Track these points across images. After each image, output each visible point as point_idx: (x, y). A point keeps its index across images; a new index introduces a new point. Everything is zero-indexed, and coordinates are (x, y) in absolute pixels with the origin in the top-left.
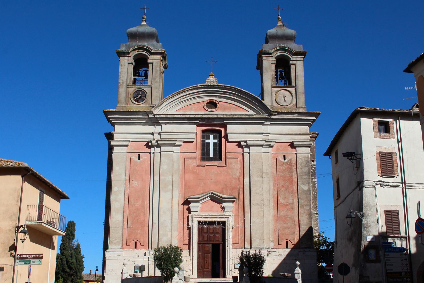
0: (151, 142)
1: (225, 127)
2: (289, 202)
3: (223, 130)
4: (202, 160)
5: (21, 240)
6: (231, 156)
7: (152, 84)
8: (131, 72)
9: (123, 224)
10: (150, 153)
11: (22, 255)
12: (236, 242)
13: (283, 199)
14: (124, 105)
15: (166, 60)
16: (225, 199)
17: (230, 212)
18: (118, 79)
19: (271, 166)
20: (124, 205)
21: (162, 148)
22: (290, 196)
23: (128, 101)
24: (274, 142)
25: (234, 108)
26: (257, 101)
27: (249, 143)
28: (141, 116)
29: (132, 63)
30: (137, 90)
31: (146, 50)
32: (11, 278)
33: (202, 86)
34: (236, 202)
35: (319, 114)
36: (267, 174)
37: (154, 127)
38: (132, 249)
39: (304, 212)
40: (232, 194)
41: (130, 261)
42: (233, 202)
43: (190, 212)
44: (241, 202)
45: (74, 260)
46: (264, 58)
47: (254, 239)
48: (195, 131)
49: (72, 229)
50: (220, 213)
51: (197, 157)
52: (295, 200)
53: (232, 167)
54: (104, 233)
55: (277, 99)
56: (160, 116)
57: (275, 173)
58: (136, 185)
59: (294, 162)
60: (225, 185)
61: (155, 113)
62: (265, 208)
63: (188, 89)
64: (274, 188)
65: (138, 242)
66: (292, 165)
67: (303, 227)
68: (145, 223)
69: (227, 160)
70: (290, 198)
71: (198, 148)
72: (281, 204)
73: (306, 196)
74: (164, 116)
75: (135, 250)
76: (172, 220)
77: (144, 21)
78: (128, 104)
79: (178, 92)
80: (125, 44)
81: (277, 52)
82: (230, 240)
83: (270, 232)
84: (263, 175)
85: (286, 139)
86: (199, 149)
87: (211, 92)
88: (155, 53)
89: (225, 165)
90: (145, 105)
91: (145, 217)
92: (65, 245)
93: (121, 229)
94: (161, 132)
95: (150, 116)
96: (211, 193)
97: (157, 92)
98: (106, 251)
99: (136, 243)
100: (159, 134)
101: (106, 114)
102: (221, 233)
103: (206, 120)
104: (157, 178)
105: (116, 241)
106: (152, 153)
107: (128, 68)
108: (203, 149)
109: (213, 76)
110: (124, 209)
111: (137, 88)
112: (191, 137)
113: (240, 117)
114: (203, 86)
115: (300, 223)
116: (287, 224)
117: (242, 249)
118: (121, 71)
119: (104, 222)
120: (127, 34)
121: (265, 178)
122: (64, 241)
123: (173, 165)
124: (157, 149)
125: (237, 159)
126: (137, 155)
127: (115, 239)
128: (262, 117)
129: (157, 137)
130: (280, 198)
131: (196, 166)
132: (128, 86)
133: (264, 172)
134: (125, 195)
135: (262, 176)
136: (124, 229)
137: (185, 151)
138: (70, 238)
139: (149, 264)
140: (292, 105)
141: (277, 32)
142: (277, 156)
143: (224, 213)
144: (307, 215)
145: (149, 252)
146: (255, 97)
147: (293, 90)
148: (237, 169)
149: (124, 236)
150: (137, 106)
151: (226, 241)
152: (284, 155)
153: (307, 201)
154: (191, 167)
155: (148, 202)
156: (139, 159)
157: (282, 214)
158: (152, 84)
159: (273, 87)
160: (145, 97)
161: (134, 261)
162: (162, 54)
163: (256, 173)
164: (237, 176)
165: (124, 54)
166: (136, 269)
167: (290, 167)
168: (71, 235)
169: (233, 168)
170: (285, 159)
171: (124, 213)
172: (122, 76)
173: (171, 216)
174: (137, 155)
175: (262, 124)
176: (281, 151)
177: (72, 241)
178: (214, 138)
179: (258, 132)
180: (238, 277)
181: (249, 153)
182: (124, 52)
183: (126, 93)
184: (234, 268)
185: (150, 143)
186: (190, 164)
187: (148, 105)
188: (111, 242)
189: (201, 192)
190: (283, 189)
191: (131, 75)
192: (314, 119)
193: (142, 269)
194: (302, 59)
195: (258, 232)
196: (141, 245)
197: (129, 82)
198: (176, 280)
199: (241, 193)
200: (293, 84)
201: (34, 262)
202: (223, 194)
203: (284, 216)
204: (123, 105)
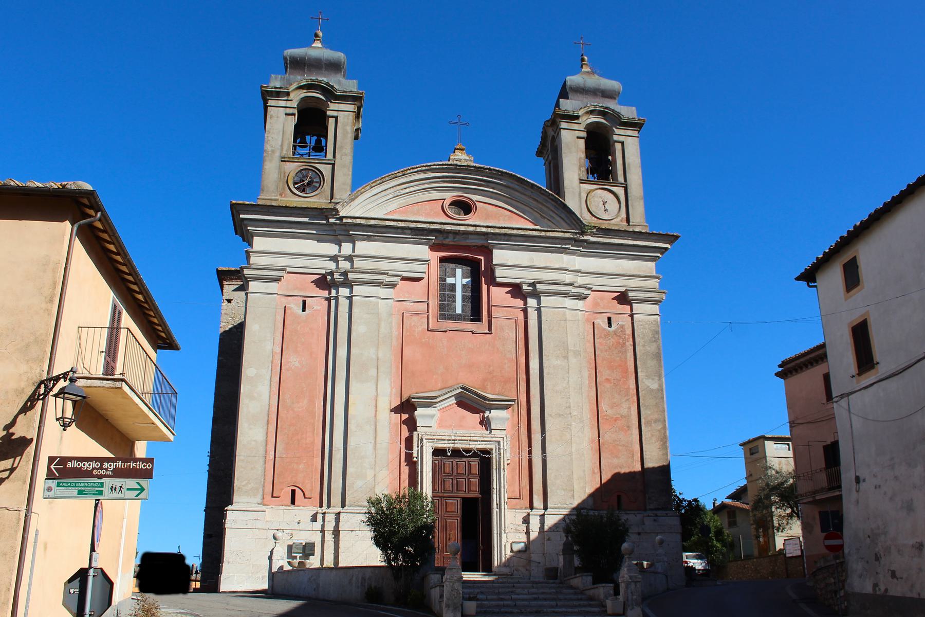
2: (621, 413)
4: (439, 319)
5: (57, 420)
9: (266, 449)
10: (329, 299)
11: (71, 459)
13: (608, 405)
14: (274, 196)
16: (491, 403)
18: (264, 143)
19: (582, 337)
20: (269, 409)
23: (284, 189)
24: (590, 289)
25: (506, 216)
26: (555, 204)
27: (539, 287)
30: (302, 168)
32: (14, 557)
34: (513, 410)
36: (577, 354)
38: (285, 506)
39: (652, 436)
40: (504, 392)
44: (523, 410)
46: (563, 125)
47: (553, 488)
48: (427, 258)
50: (479, 432)
51: (430, 311)
53: (503, 336)
54: (209, 475)
55: (590, 205)
56: (354, 221)
58: (297, 364)
59: (629, 331)
60: (490, 373)
61: (342, 214)
62: (573, 423)
63: (414, 171)
65: (298, 491)
66: (625, 337)
68: (315, 449)
72: (605, 417)
74: (363, 222)
75: (292, 507)
76: (376, 444)
77: (318, 40)
78: (283, 196)
79: (392, 174)
80: (280, 76)
81: (588, 115)
82: (502, 489)
83: (585, 475)
84: (569, 354)
85: (613, 284)
86: (433, 295)
88: (344, 98)
89: (487, 331)
90: (319, 199)
91: (315, 435)
93: (262, 461)
95: (332, 220)
96: (462, 388)
98: (226, 508)
99: (293, 492)
100: (350, 259)
101: (236, 209)
108: (442, 298)
109: (462, 150)
111: (303, 164)
114: (445, 167)
117: (528, 511)
118: (270, 129)
119: (208, 452)
120: (285, 59)
121: (573, 360)
123: (379, 325)
124: (344, 291)
125: (514, 321)
127: (246, 481)
129: (344, 265)
130: (604, 405)
131: (428, 331)
132: (283, 160)
134: (272, 386)
135: (566, 357)
137: (405, 297)
140: (619, 219)
141: (585, 81)
142: (595, 319)
146: (552, 195)
147: (620, 191)
148: (515, 339)
150: (302, 199)
153: (657, 412)
154: (416, 332)
156: (304, 310)
160: (318, 184)
162: (356, 99)
165: (278, 94)
167: (621, 341)
170: (610, 325)
171: (268, 424)
172: (272, 138)
176: (603, 308)
179: (557, 266)
182: (279, 90)
183: (280, 173)
186: (414, 325)
187: (326, 199)
188: (239, 488)
189: (439, 386)
190: (608, 385)
191: (290, 137)
192: (666, 249)
193: (308, 550)
194: (636, 134)
197: (286, 151)
200: (621, 179)
201: (118, 490)
202: (485, 391)
203: (612, 442)
204: (272, 196)
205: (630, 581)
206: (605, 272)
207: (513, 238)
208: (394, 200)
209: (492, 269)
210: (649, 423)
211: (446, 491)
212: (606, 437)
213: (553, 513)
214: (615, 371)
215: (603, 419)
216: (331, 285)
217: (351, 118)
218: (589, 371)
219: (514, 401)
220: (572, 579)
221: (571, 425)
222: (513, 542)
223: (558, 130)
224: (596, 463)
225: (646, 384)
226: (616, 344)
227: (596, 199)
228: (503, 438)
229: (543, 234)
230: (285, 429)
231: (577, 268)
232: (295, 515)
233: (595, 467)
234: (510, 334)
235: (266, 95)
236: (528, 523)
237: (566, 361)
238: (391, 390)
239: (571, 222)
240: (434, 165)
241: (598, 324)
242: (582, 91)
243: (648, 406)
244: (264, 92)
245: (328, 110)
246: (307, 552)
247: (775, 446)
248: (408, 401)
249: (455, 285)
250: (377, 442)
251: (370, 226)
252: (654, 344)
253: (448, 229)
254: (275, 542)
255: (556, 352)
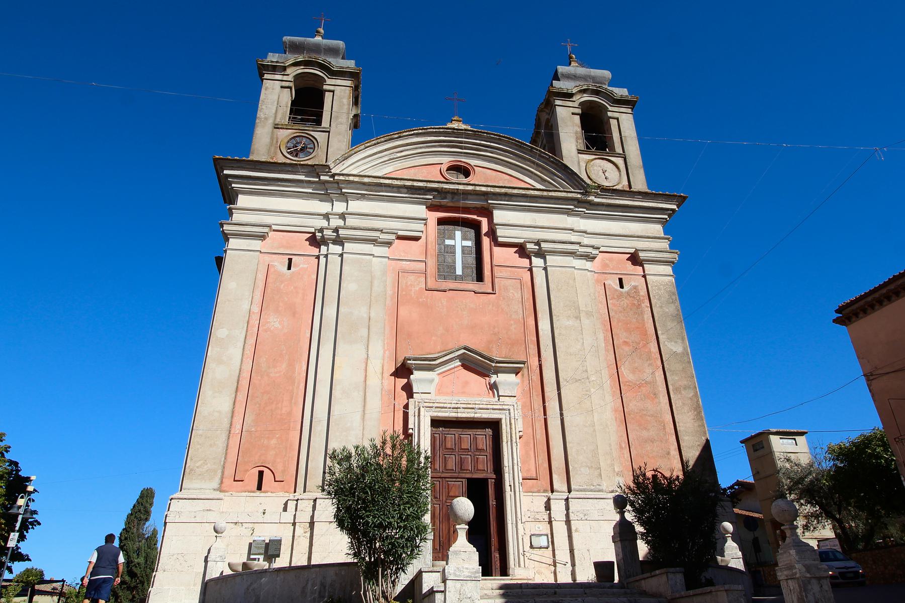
0: (321, 230)
1: (489, 215)
3: (484, 222)
6: (504, 273)
7: (330, 126)
8: (287, 103)
10: (318, 257)
12: (528, 476)
13: (629, 370)
15: (360, 105)
17: (511, 396)
19: (594, 298)
20: (240, 374)
21: (348, 246)
22: (646, 365)
23: (275, 153)
26: (556, 167)
28: (302, 177)
29: (290, 88)
31: (322, 67)
33: (440, 130)
34: (523, 375)
35: (684, 198)
36: (589, 314)
37: (329, 203)
38: (249, 492)
39: (684, 404)
41: (238, 527)
42: (517, 372)
43: (410, 395)
45: (141, 560)
47: (576, 466)
48: (424, 216)
49: (147, 501)
50: (485, 400)
51: (428, 270)
52: (657, 374)
57: (605, 314)
58: (277, 325)
59: (643, 292)
60: (495, 334)
61: (333, 171)
63: (410, 133)
64: (607, 346)
65: (267, 473)
67: (686, 438)
69: (496, 280)
70: (647, 371)
71: (429, 253)
72: (628, 383)
73: (681, 367)
75: (258, 493)
77: (320, 35)
82: (516, 467)
87: (458, 144)
89: (492, 292)
92: (129, 532)
93: (224, 437)
94: (346, 212)
95: (322, 178)
96: (465, 349)
97: (339, 141)
99: (261, 474)
102: (489, 451)
103: (449, 196)
104: (330, 311)
105: (205, 467)
106: (321, 257)
107: (281, 95)
110: (238, 383)
112: (415, 228)
113: (523, 193)
114: (442, 130)
115: (678, 429)
116: (648, 430)
117: (547, 494)
118: (265, 99)
121: (586, 322)
122: (129, 523)
124: (335, 249)
126: (284, 260)
128: (570, 195)
129: (336, 222)
131: (426, 290)
132: (276, 127)
133: (583, 311)
134: (246, 349)
135: (578, 318)
136: (231, 435)
138: (140, 517)
139: (294, 536)
142: (605, 280)
143: (497, 398)
144: (691, 411)
145: (297, 500)
147: (620, 161)
148: (520, 300)
149: (228, 455)
151: (506, 470)
152: (619, 278)
153: (685, 377)
154: (413, 291)
155: (305, 368)
156: (289, 268)
157: (632, 405)
158: (330, 126)
159: (580, 152)
160: (312, 150)
161: (251, 525)
163: (565, 311)
164: (521, 316)
165: (274, 69)
166: (253, 550)
167: (636, 302)
168: (143, 511)
169: (511, 298)
170: (622, 286)
173: (363, 403)
174: (284, 260)
175: (568, 213)
176: (613, 269)
177: (144, 524)
178: (464, 238)
180: (613, 563)
181: (545, 269)
182: (276, 64)
183: (272, 138)
184: (532, 547)
185: (320, 234)
186: (411, 285)
188: (191, 470)
189: (439, 348)
190: (626, 349)
192: (673, 210)
193: (271, 549)
194: (630, 111)
195: (585, 448)
196: (275, 481)
198: (466, 566)
199: (533, 355)
200: (619, 150)
203: (639, 411)
205: (808, 575)
206: (611, 233)
207: (514, 198)
208: (390, 163)
209: (493, 229)
210: (677, 390)
211: (448, 470)
212: (631, 406)
213: (578, 496)
214: (632, 333)
215: (625, 385)
216: (320, 243)
217: (348, 92)
218: (604, 333)
219: (524, 363)
220: (644, 579)
221: (589, 391)
222: (533, 535)
223: (553, 107)
224: (622, 436)
225: (668, 347)
226: (630, 305)
227: (595, 168)
228: (514, 405)
229: (545, 193)
230: (257, 397)
231: (582, 228)
232: (260, 504)
233: (621, 441)
234: (516, 295)
235: (263, 69)
236: (550, 510)
237: (578, 321)
238: (384, 352)
239: (573, 183)
240: (430, 128)
241: (609, 285)
242: (574, 77)
243: (674, 371)
244: (260, 66)
245: (325, 84)
246: (270, 552)
247: (781, 441)
248: (404, 364)
249: (454, 246)
250: (366, 412)
251: (364, 184)
252: (672, 305)
253: (446, 188)
254: (216, 536)
255: (566, 312)
